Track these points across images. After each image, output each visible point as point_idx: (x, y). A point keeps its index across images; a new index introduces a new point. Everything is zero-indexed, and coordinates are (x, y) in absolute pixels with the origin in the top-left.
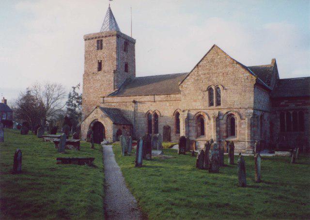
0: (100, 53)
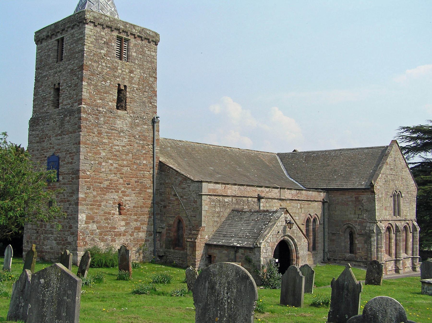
0: (122, 68)
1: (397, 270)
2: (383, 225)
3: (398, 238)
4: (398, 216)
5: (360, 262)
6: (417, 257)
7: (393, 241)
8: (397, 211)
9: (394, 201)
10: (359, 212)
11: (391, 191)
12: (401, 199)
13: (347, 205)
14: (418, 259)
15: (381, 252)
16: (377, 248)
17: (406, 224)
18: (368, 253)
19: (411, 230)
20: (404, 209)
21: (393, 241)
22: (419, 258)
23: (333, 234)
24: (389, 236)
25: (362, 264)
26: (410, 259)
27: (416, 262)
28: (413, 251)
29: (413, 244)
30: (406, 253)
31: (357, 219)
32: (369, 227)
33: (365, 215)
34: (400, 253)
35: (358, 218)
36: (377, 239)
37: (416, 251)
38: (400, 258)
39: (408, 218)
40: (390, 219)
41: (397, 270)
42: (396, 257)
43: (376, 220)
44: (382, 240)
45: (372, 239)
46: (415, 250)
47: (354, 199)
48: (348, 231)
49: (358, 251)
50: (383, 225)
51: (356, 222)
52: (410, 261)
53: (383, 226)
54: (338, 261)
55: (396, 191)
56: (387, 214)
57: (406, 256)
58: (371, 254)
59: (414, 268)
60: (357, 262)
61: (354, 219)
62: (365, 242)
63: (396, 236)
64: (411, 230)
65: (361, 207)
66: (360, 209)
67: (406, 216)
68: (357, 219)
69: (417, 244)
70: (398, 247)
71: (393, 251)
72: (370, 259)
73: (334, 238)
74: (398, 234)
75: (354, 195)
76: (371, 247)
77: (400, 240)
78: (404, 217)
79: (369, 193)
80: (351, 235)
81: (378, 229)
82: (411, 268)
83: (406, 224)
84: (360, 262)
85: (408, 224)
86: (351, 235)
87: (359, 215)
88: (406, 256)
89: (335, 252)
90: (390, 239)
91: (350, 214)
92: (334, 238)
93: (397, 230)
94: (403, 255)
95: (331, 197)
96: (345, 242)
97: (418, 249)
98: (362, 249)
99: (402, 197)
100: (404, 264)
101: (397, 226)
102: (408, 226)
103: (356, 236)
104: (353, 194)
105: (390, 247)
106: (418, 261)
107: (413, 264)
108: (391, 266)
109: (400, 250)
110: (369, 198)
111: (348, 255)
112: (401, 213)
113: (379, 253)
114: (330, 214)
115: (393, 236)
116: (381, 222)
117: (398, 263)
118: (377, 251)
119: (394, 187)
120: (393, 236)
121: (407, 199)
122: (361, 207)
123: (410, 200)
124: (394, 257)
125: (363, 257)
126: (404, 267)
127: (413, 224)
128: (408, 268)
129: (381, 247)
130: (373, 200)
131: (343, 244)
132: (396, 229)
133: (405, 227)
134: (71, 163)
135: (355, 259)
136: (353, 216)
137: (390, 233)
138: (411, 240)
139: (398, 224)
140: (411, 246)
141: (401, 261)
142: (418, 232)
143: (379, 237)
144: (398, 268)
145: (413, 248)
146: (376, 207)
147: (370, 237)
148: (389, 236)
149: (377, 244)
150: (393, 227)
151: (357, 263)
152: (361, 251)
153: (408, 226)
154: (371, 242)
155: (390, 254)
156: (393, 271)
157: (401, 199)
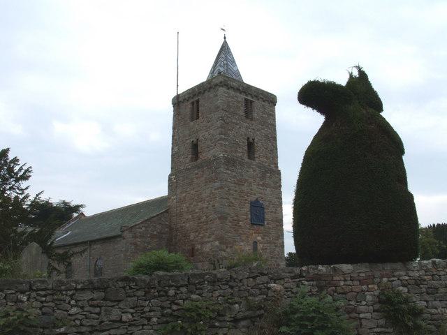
134: (275, 213)
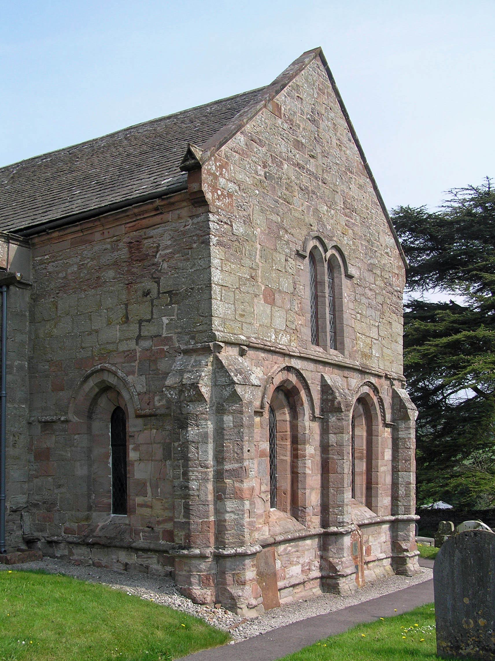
1: (329, 581)
2: (257, 376)
3: (332, 438)
4: (332, 351)
5: (145, 550)
6: (409, 521)
7: (311, 450)
8: (327, 324)
9: (316, 283)
10: (140, 310)
11: (300, 234)
12: (346, 282)
13: (98, 283)
14: (413, 526)
15: (238, 496)
16: (219, 476)
17: (366, 389)
18: (173, 508)
19: (388, 417)
20: (358, 326)
21: (311, 450)
22: (417, 521)
23: (47, 425)
24: (294, 427)
25: (154, 563)
26: (386, 527)
27: (406, 539)
28: (395, 498)
29: (395, 471)
30: (369, 505)
31: (132, 345)
32: (181, 373)
33: (165, 320)
34: (341, 505)
35: (139, 338)
36: (220, 432)
37: (408, 495)
38: (341, 524)
39: (375, 366)
40: (295, 348)
41: (329, 581)
42: (325, 524)
43: (214, 338)
44: (240, 435)
45: (192, 432)
46: (402, 491)
47: (124, 253)
48: (105, 407)
49: (139, 500)
50: (257, 376)
51: (130, 356)
52: (384, 534)
53: (256, 375)
54: (61, 551)
55: (318, 238)
56: (279, 322)
57: (367, 515)
58: (187, 509)
59: (399, 564)
60: (137, 550)
61: (123, 347)
62: (167, 454)
63: (325, 431)
64: (388, 417)
65: (149, 284)
66: (146, 294)
67: (365, 355)
68: (132, 345)
69: (408, 471)
70: (332, 477)
71: (313, 498)
72: (182, 533)
73: (50, 442)
74: (333, 419)
75: (122, 231)
76: (185, 474)
77: (340, 445)
78: (358, 356)
79: (184, 212)
80: (118, 419)
81: (222, 380)
82: (387, 563)
83: (366, 389)
84: (145, 550)
85: (376, 390)
86: (118, 419)
87: (140, 322)
88: (367, 515)
89: (50, 506)
90: (296, 441)
91: (109, 323)
92: (50, 442)
93: (330, 404)
94: (355, 513)
95: (42, 262)
96: (87, 459)
97: (413, 486)
98: (154, 487)
99: (350, 277)
100: (358, 550)
101: (326, 389)
102: (375, 400)
103: (133, 425)
104: (123, 229)
105: (296, 476)
106: (412, 533)
107: (395, 545)
108: (299, 564)
109: (340, 491)
110: (184, 233)
111: (105, 520)
112: (347, 342)
113: (230, 505)
114: (37, 337)
115: (311, 428)
116: (242, 353)
117: (332, 549)
118: (220, 496)
119: (310, 219)
120: (311, 428)
121: (370, 293)
122: (149, 284)
123: (380, 299)
124: (314, 524)
125: (159, 528)
126: (360, 561)
127: (395, 395)
128: (380, 568)
129: (239, 474)
130: (200, 240)
131: (81, 471)
132: (323, 401)
133: (363, 400)
135: (127, 539)
136: (115, 332)
137: (295, 414)
138: (388, 455)
139: (333, 378)
140: (388, 479)
141: (347, 541)
142: (412, 423)
143: (228, 419)
144: (332, 567)
145: (395, 485)
146: (216, 276)
147: (182, 423)
148: (294, 427)
149: (219, 458)
150: (307, 388)
151: (133, 559)
152: (148, 499)
153: (375, 400)
154: (185, 445)
155: (297, 510)
156: (308, 586)
157: (346, 282)
